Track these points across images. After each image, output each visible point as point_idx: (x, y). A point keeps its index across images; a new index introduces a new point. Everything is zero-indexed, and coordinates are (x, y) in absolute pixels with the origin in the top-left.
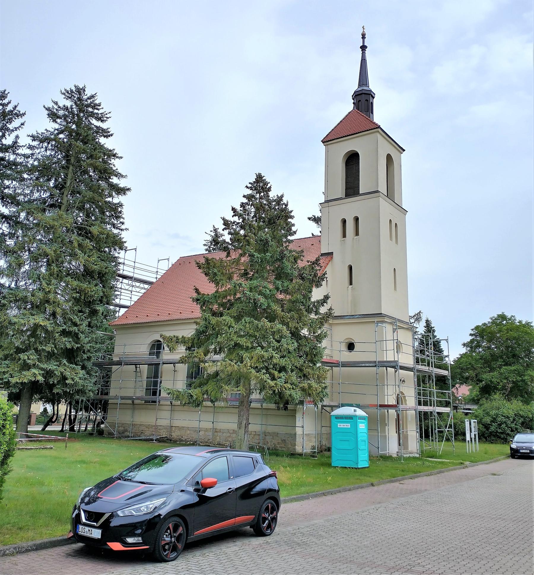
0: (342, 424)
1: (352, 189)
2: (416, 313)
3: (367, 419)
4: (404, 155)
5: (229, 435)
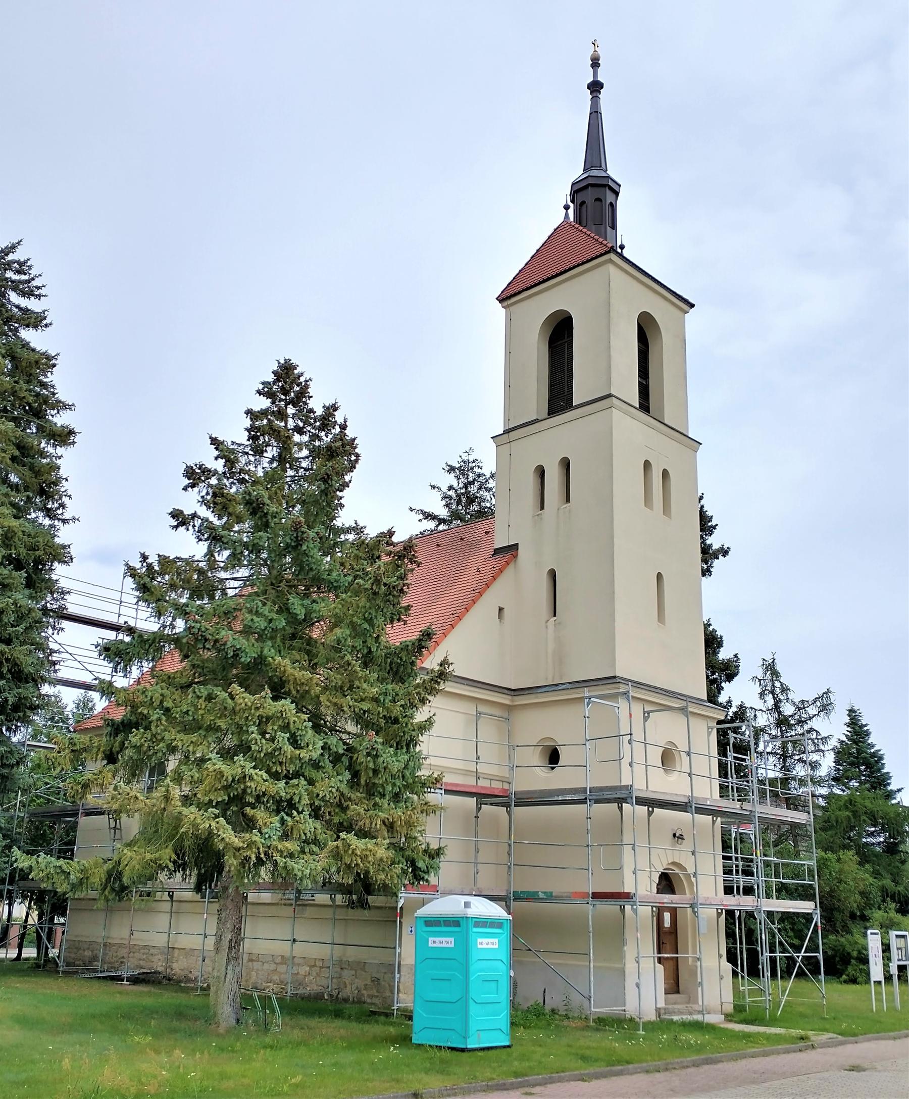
0: (437, 939)
1: (560, 397)
2: (821, 694)
3: (507, 927)
4: (691, 317)
5: (273, 967)
